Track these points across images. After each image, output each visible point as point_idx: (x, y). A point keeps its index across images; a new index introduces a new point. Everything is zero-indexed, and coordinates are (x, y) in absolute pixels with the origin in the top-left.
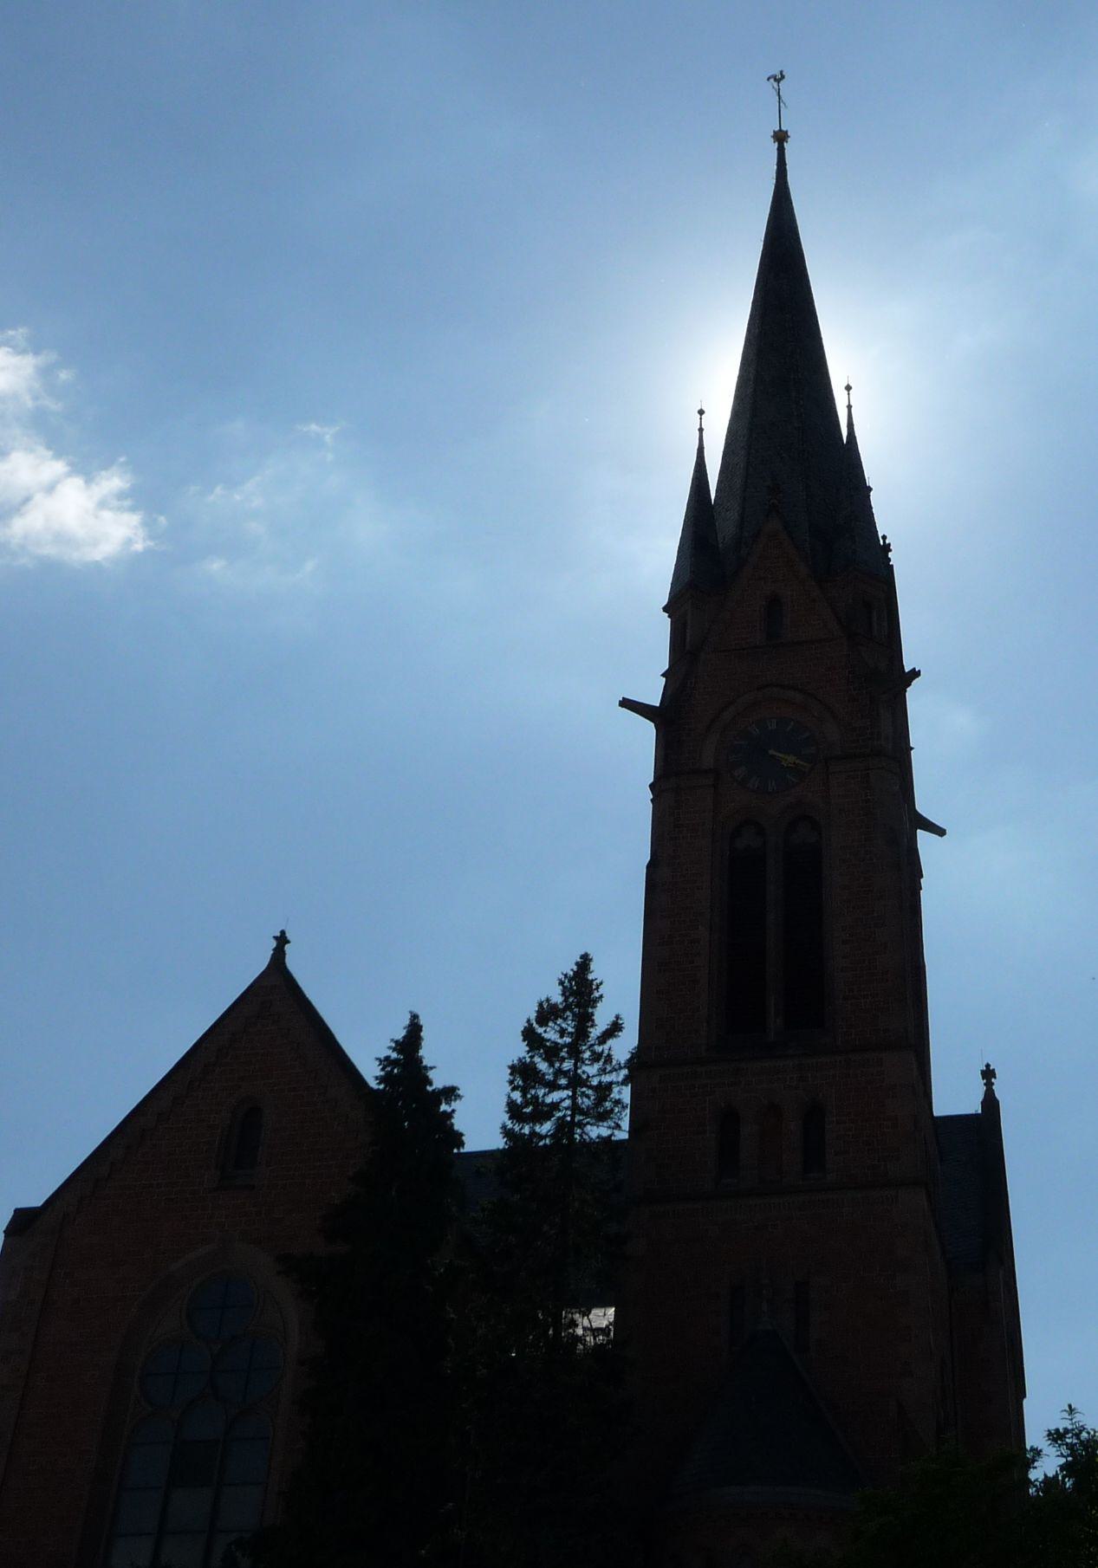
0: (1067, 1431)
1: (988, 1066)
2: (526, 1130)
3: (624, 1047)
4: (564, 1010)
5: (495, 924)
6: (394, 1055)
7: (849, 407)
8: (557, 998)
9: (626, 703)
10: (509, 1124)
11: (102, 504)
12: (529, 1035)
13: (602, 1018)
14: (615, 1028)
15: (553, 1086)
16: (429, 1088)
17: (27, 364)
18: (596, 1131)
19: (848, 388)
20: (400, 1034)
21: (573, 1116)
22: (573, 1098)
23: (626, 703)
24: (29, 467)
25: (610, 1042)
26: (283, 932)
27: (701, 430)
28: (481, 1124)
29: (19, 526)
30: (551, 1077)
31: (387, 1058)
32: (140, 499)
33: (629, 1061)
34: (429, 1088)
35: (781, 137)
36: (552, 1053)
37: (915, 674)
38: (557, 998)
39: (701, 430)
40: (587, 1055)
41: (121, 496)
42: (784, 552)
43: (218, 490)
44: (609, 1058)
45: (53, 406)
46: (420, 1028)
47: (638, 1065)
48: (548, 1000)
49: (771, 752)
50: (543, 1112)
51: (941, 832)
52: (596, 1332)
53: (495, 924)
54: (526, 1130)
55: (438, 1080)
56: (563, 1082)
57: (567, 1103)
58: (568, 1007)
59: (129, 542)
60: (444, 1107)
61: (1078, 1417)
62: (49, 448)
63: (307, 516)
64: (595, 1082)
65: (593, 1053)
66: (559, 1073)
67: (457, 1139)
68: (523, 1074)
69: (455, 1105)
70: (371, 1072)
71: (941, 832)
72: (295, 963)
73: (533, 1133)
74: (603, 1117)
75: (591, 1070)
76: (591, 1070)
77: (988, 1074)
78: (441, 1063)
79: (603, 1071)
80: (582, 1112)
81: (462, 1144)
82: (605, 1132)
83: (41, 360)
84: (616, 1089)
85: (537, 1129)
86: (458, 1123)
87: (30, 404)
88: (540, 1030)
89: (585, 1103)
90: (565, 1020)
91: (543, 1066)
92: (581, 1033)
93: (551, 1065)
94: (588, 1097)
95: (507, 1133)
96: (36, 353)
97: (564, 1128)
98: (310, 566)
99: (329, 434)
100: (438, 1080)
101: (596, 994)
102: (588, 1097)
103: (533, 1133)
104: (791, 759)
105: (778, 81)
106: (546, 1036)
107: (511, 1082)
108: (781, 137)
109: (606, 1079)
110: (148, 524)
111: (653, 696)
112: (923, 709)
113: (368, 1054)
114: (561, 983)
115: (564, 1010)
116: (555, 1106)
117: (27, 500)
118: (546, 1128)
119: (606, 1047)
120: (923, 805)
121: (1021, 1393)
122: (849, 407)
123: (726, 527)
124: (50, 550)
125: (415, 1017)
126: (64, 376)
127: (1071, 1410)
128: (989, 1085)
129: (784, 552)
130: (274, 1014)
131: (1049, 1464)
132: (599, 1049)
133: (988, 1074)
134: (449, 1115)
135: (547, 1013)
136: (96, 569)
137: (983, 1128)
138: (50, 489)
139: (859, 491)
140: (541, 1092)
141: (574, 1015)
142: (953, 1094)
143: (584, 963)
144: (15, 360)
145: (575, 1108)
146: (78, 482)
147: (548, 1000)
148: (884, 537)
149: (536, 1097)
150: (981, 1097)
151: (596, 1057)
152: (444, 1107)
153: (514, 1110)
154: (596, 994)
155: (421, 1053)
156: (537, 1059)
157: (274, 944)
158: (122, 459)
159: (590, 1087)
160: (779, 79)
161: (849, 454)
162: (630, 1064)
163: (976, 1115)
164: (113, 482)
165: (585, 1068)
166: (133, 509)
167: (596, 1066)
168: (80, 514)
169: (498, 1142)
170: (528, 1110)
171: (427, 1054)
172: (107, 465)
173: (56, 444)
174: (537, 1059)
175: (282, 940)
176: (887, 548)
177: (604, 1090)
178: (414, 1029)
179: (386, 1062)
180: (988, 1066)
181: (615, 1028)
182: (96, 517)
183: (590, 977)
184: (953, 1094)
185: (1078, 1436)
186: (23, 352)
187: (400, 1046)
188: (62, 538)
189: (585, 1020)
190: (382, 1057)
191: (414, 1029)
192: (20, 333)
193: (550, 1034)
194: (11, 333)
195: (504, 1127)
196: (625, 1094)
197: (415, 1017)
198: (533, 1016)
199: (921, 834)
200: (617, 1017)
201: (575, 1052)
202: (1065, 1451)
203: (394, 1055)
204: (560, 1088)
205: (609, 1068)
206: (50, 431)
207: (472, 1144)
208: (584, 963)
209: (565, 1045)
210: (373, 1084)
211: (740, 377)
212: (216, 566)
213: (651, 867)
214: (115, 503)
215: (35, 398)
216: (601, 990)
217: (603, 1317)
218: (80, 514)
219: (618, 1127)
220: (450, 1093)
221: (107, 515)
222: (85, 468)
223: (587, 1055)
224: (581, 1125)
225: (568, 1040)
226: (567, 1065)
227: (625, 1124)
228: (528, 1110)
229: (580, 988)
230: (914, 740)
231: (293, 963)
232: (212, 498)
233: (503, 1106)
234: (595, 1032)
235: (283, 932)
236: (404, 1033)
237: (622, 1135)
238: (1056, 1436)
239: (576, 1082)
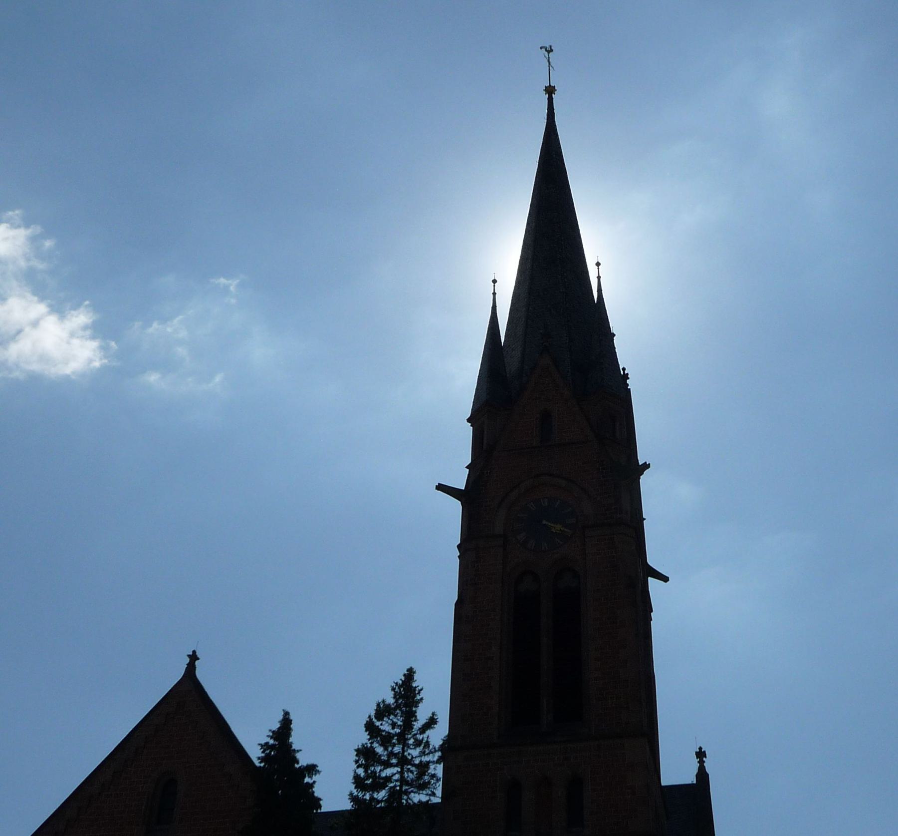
1: (700, 748)
2: (367, 797)
3: (438, 736)
5: (351, 637)
6: (272, 742)
7: (599, 278)
8: (390, 700)
9: (441, 487)
10: (355, 792)
11: (72, 335)
12: (370, 727)
13: (422, 715)
14: (432, 722)
15: (387, 765)
16: (297, 766)
17: (22, 234)
18: (418, 797)
19: (598, 264)
20: (276, 726)
21: (401, 786)
22: (401, 773)
23: (441, 487)
24: (22, 308)
25: (428, 732)
26: (194, 652)
27: (494, 294)
28: (334, 792)
29: (14, 350)
30: (385, 758)
31: (267, 744)
32: (99, 330)
33: (441, 746)
34: (297, 766)
35: (550, 91)
36: (386, 740)
37: (646, 466)
38: (390, 700)
39: (494, 294)
40: (411, 741)
41: (85, 328)
42: (554, 381)
43: (155, 325)
44: (427, 744)
45: (41, 266)
46: (290, 722)
47: (448, 747)
48: (384, 701)
49: (544, 522)
50: (379, 783)
51: (665, 579)
54: (367, 797)
55: (303, 760)
56: (394, 761)
57: (397, 777)
58: (398, 706)
59: (90, 361)
60: (307, 780)
62: (34, 293)
63: (215, 345)
64: (417, 761)
65: (416, 740)
66: (391, 754)
67: (316, 802)
68: (365, 755)
69: (315, 778)
70: (255, 753)
71: (665, 579)
73: (372, 799)
74: (423, 787)
75: (415, 752)
77: (701, 755)
78: (306, 748)
79: (423, 753)
80: (407, 783)
81: (320, 807)
82: (423, 798)
83: (29, 232)
84: (432, 767)
85: (375, 796)
86: (318, 791)
87: (23, 263)
88: (378, 723)
89: (410, 776)
90: (396, 716)
91: (379, 750)
92: (407, 725)
93: (386, 749)
94: (412, 772)
95: (353, 798)
96: (27, 226)
97: (395, 795)
98: (218, 378)
99: (233, 285)
100: (303, 760)
101: (418, 697)
102: (412, 772)
103: (372, 799)
106: (382, 727)
107: (357, 762)
108: (550, 91)
109: (425, 759)
110: (104, 348)
113: (253, 739)
114: (393, 689)
116: (388, 779)
117: (19, 332)
118: (382, 795)
119: (425, 736)
122: (599, 278)
123: (512, 363)
124: (35, 367)
125: (286, 714)
126: (48, 244)
128: (701, 763)
129: (554, 381)
130: (187, 712)
132: (420, 737)
133: (701, 755)
134: (311, 786)
135: (383, 711)
136: (67, 380)
137: (698, 794)
138: (35, 324)
140: (378, 769)
141: (402, 712)
142: (676, 770)
143: (410, 675)
144: (13, 233)
145: (403, 781)
146: (52, 319)
147: (384, 701)
148: (624, 369)
149: (374, 772)
151: (418, 743)
152: (307, 780)
153: (358, 781)
154: (418, 697)
156: (375, 745)
157: (188, 660)
158: (87, 303)
160: (550, 50)
162: (442, 748)
164: (81, 318)
165: (410, 751)
166: (93, 338)
167: (418, 750)
168: (58, 342)
169: (348, 805)
170: (369, 782)
171: (296, 740)
172: (76, 307)
173: (40, 291)
174: (375, 745)
175: (194, 657)
176: (626, 377)
177: (423, 767)
179: (265, 746)
180: (700, 748)
181: (432, 722)
182: (68, 343)
184: (676, 770)
186: (19, 227)
188: (44, 358)
189: (410, 716)
190: (263, 742)
192: (16, 214)
194: (10, 213)
195: (351, 794)
197: (286, 714)
198: (373, 713)
199: (652, 582)
200: (433, 714)
201: (402, 739)
203: (272, 742)
204: (392, 765)
205: (427, 751)
206: (36, 284)
207: (326, 807)
208: (410, 675)
209: (396, 734)
210: (257, 763)
212: (153, 378)
214: (81, 333)
215: (28, 260)
216: (422, 694)
218: (58, 342)
219: (434, 794)
220: (312, 769)
221: (76, 342)
222: (59, 309)
223: (411, 741)
224: (407, 793)
225: (398, 730)
226: (397, 749)
227: (439, 792)
228: (369, 782)
229: (407, 693)
231: (200, 674)
232: (150, 330)
234: (417, 725)
235: (194, 652)
236: (278, 725)
237: (437, 800)
239: (403, 761)
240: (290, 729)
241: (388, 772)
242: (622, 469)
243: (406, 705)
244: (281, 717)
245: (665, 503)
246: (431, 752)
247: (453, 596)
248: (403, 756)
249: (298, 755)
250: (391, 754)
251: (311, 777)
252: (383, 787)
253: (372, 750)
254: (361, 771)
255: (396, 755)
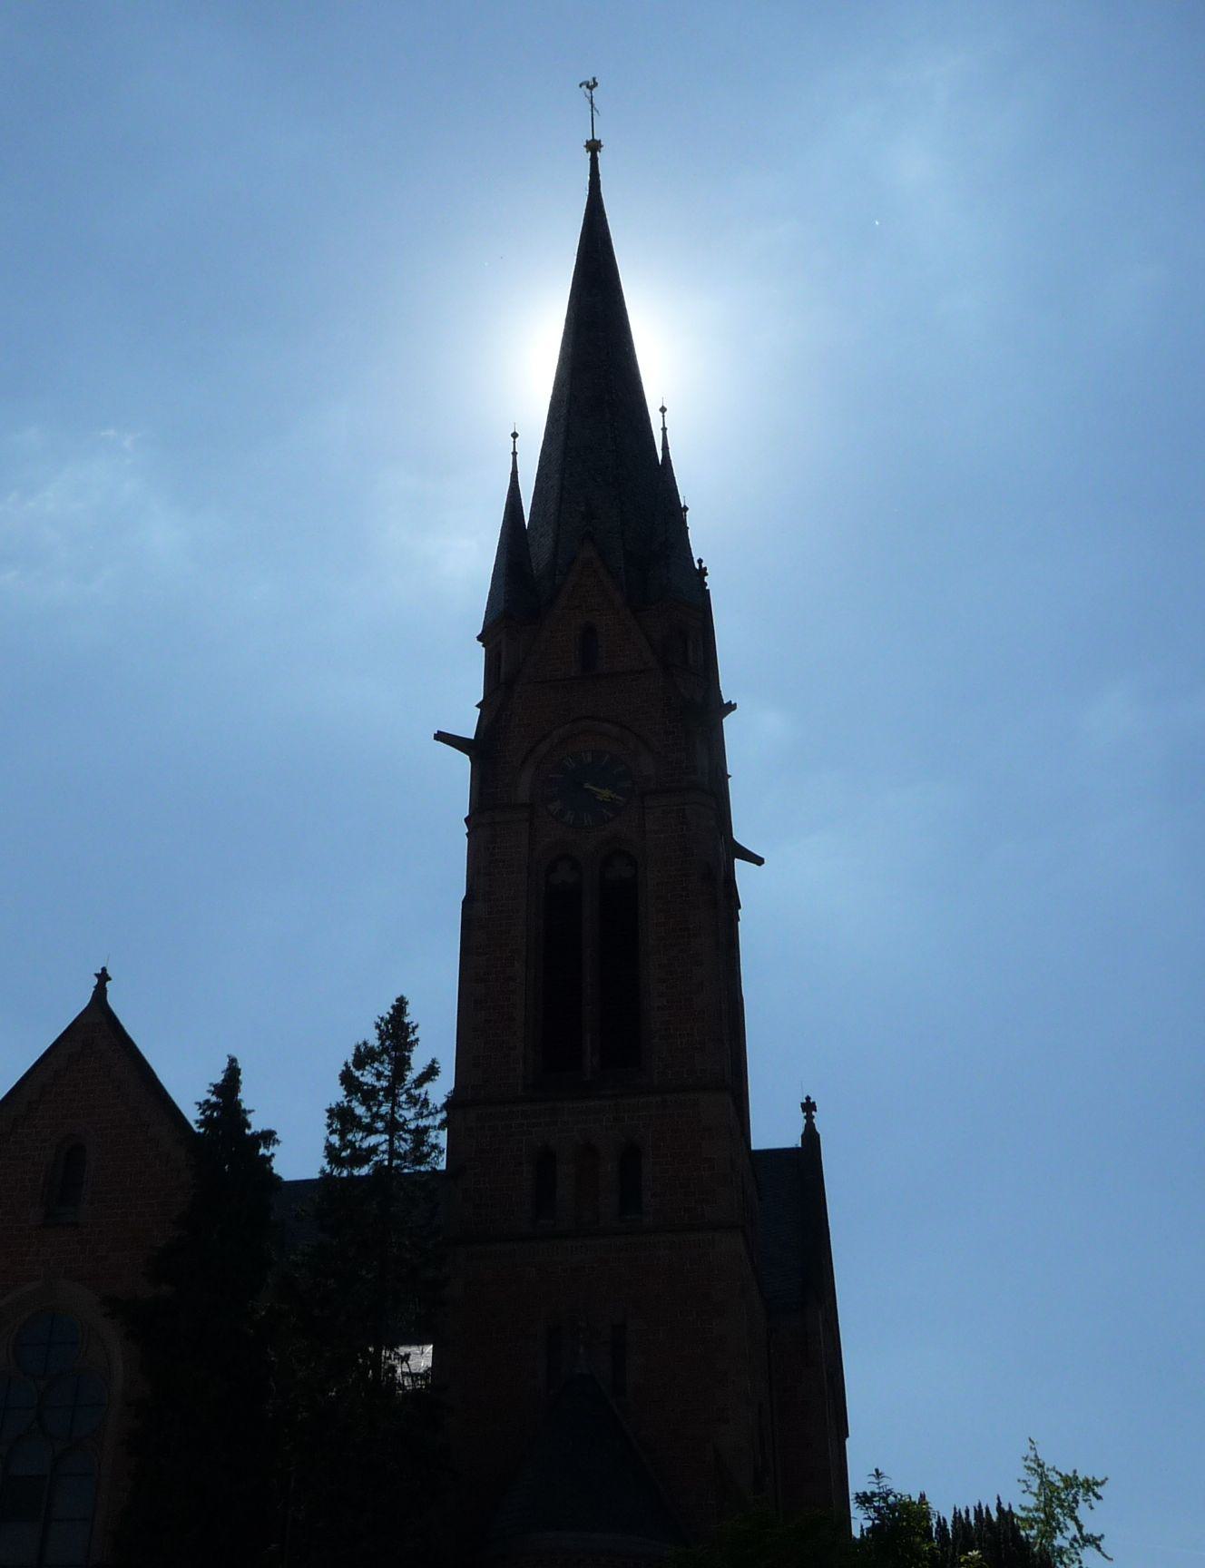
0: (874, 1494)
1: (808, 1098)
3: (440, 1090)
4: (381, 1054)
5: (309, 970)
6: (214, 1099)
7: (664, 429)
8: (374, 1042)
9: (441, 737)
12: (347, 1079)
14: (431, 1072)
15: (370, 1130)
19: (663, 410)
20: (219, 1078)
21: (390, 1161)
22: (391, 1142)
23: (441, 737)
25: (427, 1086)
26: (104, 970)
27: (514, 454)
28: (299, 1156)
31: (207, 1101)
35: (594, 147)
36: (369, 1096)
38: (374, 1042)
39: (514, 454)
40: (403, 1098)
42: (601, 573)
44: (426, 1103)
47: (451, 1104)
49: (587, 786)
51: (759, 861)
52: (414, 1376)
53: (309, 970)
54: (345, 1174)
55: (257, 1124)
56: (380, 1125)
57: (384, 1147)
58: (385, 1050)
60: (262, 1151)
61: (884, 1482)
64: (412, 1126)
65: (410, 1096)
66: (376, 1116)
68: (342, 1118)
69: (273, 1149)
70: (192, 1115)
71: (759, 861)
72: (117, 1001)
76: (408, 1114)
77: (809, 1107)
78: (260, 1112)
79: (420, 1115)
84: (433, 1133)
88: (357, 1074)
89: (404, 1147)
90: (382, 1063)
91: (360, 1110)
93: (369, 1109)
100: (257, 1124)
101: (412, 1038)
104: (605, 794)
105: (591, 88)
107: (329, 1126)
108: (594, 147)
109: (423, 1123)
111: (468, 730)
112: (744, 742)
113: (189, 1092)
114: (378, 1026)
115: (381, 1054)
116: (373, 1150)
119: (422, 1091)
120: (741, 835)
121: (844, 1432)
122: (664, 429)
123: (541, 553)
125: (233, 1061)
127: (878, 1474)
128: (809, 1118)
129: (601, 573)
130: (96, 1047)
131: (860, 1521)
132: (415, 1092)
133: (809, 1107)
134: (269, 1159)
135: (364, 1057)
137: (804, 1163)
139: (674, 514)
142: (772, 1129)
143: (400, 1007)
145: (393, 1153)
148: (700, 561)
150: (801, 1130)
151: (413, 1101)
152: (262, 1151)
153: (332, 1154)
154: (412, 1038)
155: (240, 1096)
156: (355, 1104)
157: (96, 981)
159: (409, 1131)
160: (592, 86)
161: (661, 476)
162: (446, 1106)
163: (797, 1149)
167: (413, 1111)
171: (246, 1097)
174: (355, 1104)
175: (103, 977)
176: (703, 572)
177: (420, 1133)
178: (233, 1073)
180: (808, 1098)
181: (431, 1072)
183: (406, 1020)
184: (772, 1129)
185: (885, 1499)
187: (218, 1090)
189: (401, 1064)
191: (233, 1073)
193: (367, 1077)
196: (441, 1138)
197: (233, 1061)
200: (434, 1061)
201: (391, 1093)
202: (873, 1514)
203: (214, 1099)
204: (376, 1131)
208: (400, 1007)
209: (382, 1089)
211: (554, 397)
213: (467, 903)
216: (418, 1033)
217: (421, 1358)
220: (268, 1137)
223: (403, 1098)
225: (385, 1084)
226: (385, 1109)
229: (397, 1031)
230: (732, 765)
231: (114, 1000)
233: (321, 1151)
234: (411, 1076)
235: (104, 970)
236: (222, 1077)
238: (865, 1499)
239: (394, 1127)
240: (238, 1082)
241: (373, 1140)
242: (694, 705)
243: (395, 1048)
244: (226, 1066)
245: (756, 747)
246: (431, 1114)
247: (458, 889)
248: (393, 1118)
249: (250, 1118)
250: (376, 1116)
251: (267, 1148)
252: (366, 1160)
253: (350, 1110)
254: (335, 1139)
255: (382, 1117)
